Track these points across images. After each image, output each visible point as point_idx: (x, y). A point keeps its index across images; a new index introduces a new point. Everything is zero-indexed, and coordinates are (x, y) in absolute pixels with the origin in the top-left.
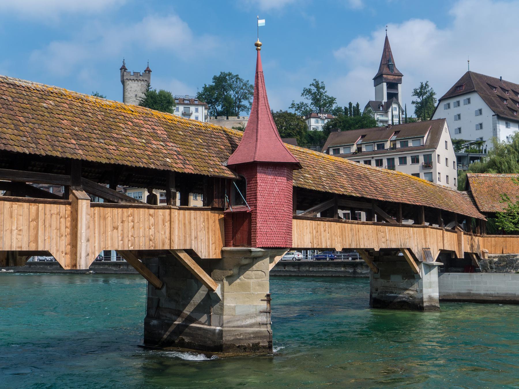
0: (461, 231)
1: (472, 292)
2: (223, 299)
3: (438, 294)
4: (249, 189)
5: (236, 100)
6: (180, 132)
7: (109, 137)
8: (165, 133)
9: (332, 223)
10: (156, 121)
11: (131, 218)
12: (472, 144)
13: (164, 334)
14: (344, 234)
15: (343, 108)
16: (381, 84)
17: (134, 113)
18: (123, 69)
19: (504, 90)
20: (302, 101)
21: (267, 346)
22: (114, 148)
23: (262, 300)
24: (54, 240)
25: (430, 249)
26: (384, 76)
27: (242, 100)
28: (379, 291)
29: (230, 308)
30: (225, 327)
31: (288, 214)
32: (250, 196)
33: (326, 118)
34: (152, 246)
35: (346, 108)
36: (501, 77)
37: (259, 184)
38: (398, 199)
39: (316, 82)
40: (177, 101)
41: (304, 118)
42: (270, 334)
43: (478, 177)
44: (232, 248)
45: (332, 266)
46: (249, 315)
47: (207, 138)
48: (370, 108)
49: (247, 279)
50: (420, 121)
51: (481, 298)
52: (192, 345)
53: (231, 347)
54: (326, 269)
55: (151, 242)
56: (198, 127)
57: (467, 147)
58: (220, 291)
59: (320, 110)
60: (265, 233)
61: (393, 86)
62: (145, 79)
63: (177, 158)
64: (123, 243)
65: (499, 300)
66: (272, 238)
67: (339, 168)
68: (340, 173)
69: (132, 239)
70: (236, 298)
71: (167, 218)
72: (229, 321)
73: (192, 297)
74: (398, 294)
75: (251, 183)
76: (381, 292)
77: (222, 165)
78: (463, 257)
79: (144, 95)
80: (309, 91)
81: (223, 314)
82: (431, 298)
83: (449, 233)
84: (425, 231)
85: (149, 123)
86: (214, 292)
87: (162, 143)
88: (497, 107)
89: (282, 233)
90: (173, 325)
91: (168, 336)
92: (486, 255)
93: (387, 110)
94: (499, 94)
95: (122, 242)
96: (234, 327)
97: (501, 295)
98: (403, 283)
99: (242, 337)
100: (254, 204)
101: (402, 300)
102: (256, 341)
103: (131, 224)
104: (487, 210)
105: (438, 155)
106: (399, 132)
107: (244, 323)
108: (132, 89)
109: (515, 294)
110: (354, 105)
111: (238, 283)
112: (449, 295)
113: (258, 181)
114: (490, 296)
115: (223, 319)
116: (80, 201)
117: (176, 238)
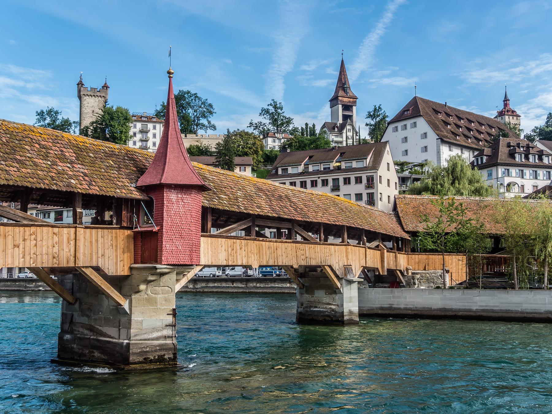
1: (393, 306)
3: (357, 308)
5: (194, 118)
6: (91, 155)
7: (12, 159)
8: (74, 155)
9: (249, 241)
10: (66, 143)
12: (415, 166)
14: (261, 251)
15: (300, 128)
17: (42, 136)
18: (80, 84)
20: (259, 121)
22: (15, 169)
23: (167, 314)
25: (351, 265)
26: (339, 98)
27: (201, 118)
28: (305, 305)
29: (137, 322)
31: (195, 233)
33: (283, 138)
34: (56, 263)
35: (302, 129)
38: (318, 219)
40: (134, 118)
41: (261, 137)
43: (404, 198)
45: (278, 283)
47: (119, 160)
48: (325, 129)
50: (373, 142)
54: (273, 285)
55: (55, 260)
56: (111, 150)
57: (411, 169)
59: (277, 129)
60: (171, 251)
62: (102, 95)
63: (82, 179)
66: (178, 256)
67: (260, 190)
68: (260, 194)
69: (34, 257)
70: (143, 313)
71: (73, 236)
77: (131, 186)
78: (386, 274)
79: (100, 110)
80: (267, 111)
82: (351, 313)
83: (372, 251)
84: (347, 249)
85: (58, 145)
87: (69, 165)
88: (441, 131)
92: (410, 271)
94: (444, 119)
95: (23, 259)
96: (141, 340)
97: (418, 309)
99: (148, 349)
102: (162, 353)
104: (411, 229)
105: (380, 177)
106: (344, 153)
108: (89, 105)
109: (431, 308)
110: (310, 125)
111: (146, 298)
112: (372, 309)
114: (409, 310)
117: (80, 255)
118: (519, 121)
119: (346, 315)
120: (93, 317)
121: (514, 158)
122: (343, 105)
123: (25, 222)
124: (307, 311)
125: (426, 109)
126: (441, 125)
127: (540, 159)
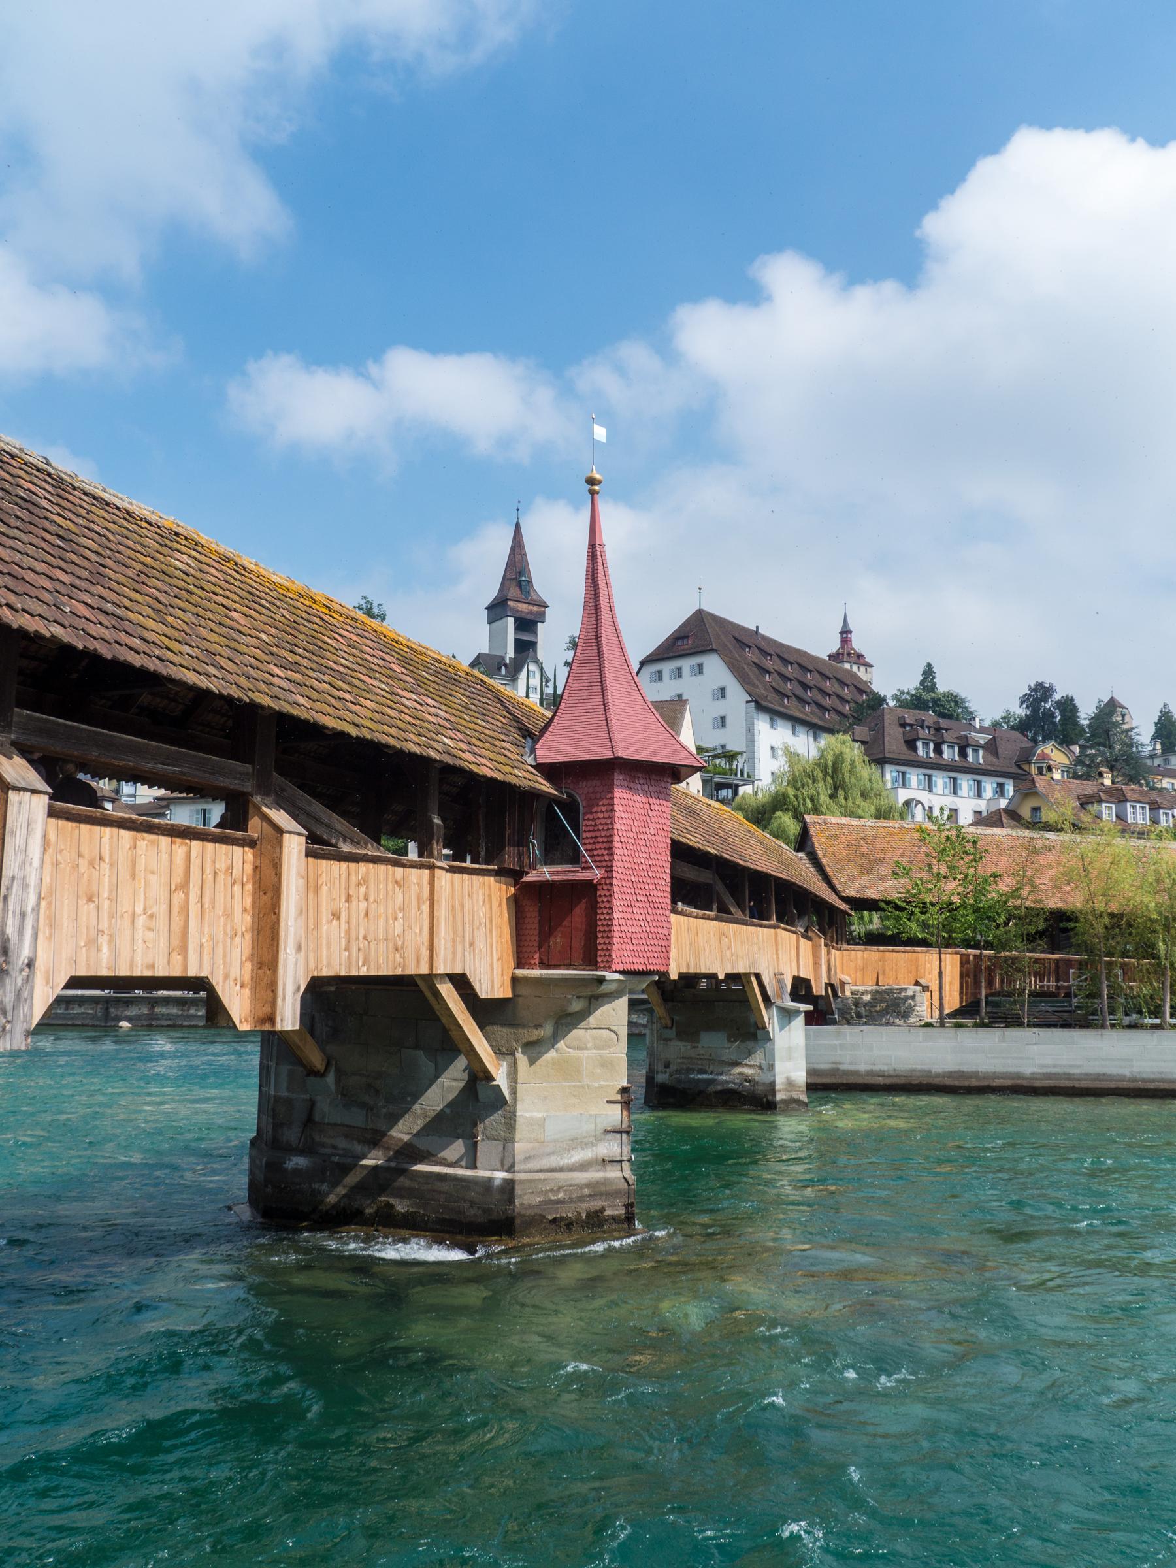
0: (820, 938)
1: (841, 1067)
2: (515, 1100)
4: (591, 825)
11: (363, 889)
13: (328, 1193)
16: (504, 620)
19: (765, 653)
21: (623, 1216)
23: (608, 1102)
24: (221, 944)
26: (510, 603)
28: (673, 1067)
30: (519, 1172)
32: (594, 843)
36: (757, 627)
37: (617, 814)
39: (367, 602)
42: (629, 1185)
43: (826, 823)
44: (536, 972)
46: (577, 1139)
49: (574, 1049)
51: (860, 1080)
52: (419, 1218)
53: (536, 1221)
58: (505, 1081)
61: (527, 625)
64: (349, 956)
65: (897, 1085)
70: (545, 1098)
72: (529, 1157)
73: (416, 1097)
74: (717, 1074)
75: (596, 812)
76: (677, 1071)
81: (514, 1139)
82: (790, 1084)
86: (494, 1083)
88: (754, 685)
89: (661, 936)
90: (358, 1168)
91: (341, 1198)
92: (847, 987)
93: (515, 675)
94: (756, 661)
95: (347, 953)
96: (541, 1171)
98: (729, 1050)
99: (561, 1195)
100: (604, 864)
101: (725, 1087)
102: (596, 1205)
103: (364, 905)
104: (853, 894)
107: (566, 1161)
109: (930, 1071)
111: (553, 1059)
113: (616, 808)
115: (514, 1150)
116: (286, 836)
117: (441, 944)
118: (869, 676)
119: (780, 1091)
120: (385, 1110)
121: (915, 749)
122: (517, 620)
123: (346, 848)
124: (679, 1081)
125: (722, 637)
126: (752, 673)
127: (963, 754)
